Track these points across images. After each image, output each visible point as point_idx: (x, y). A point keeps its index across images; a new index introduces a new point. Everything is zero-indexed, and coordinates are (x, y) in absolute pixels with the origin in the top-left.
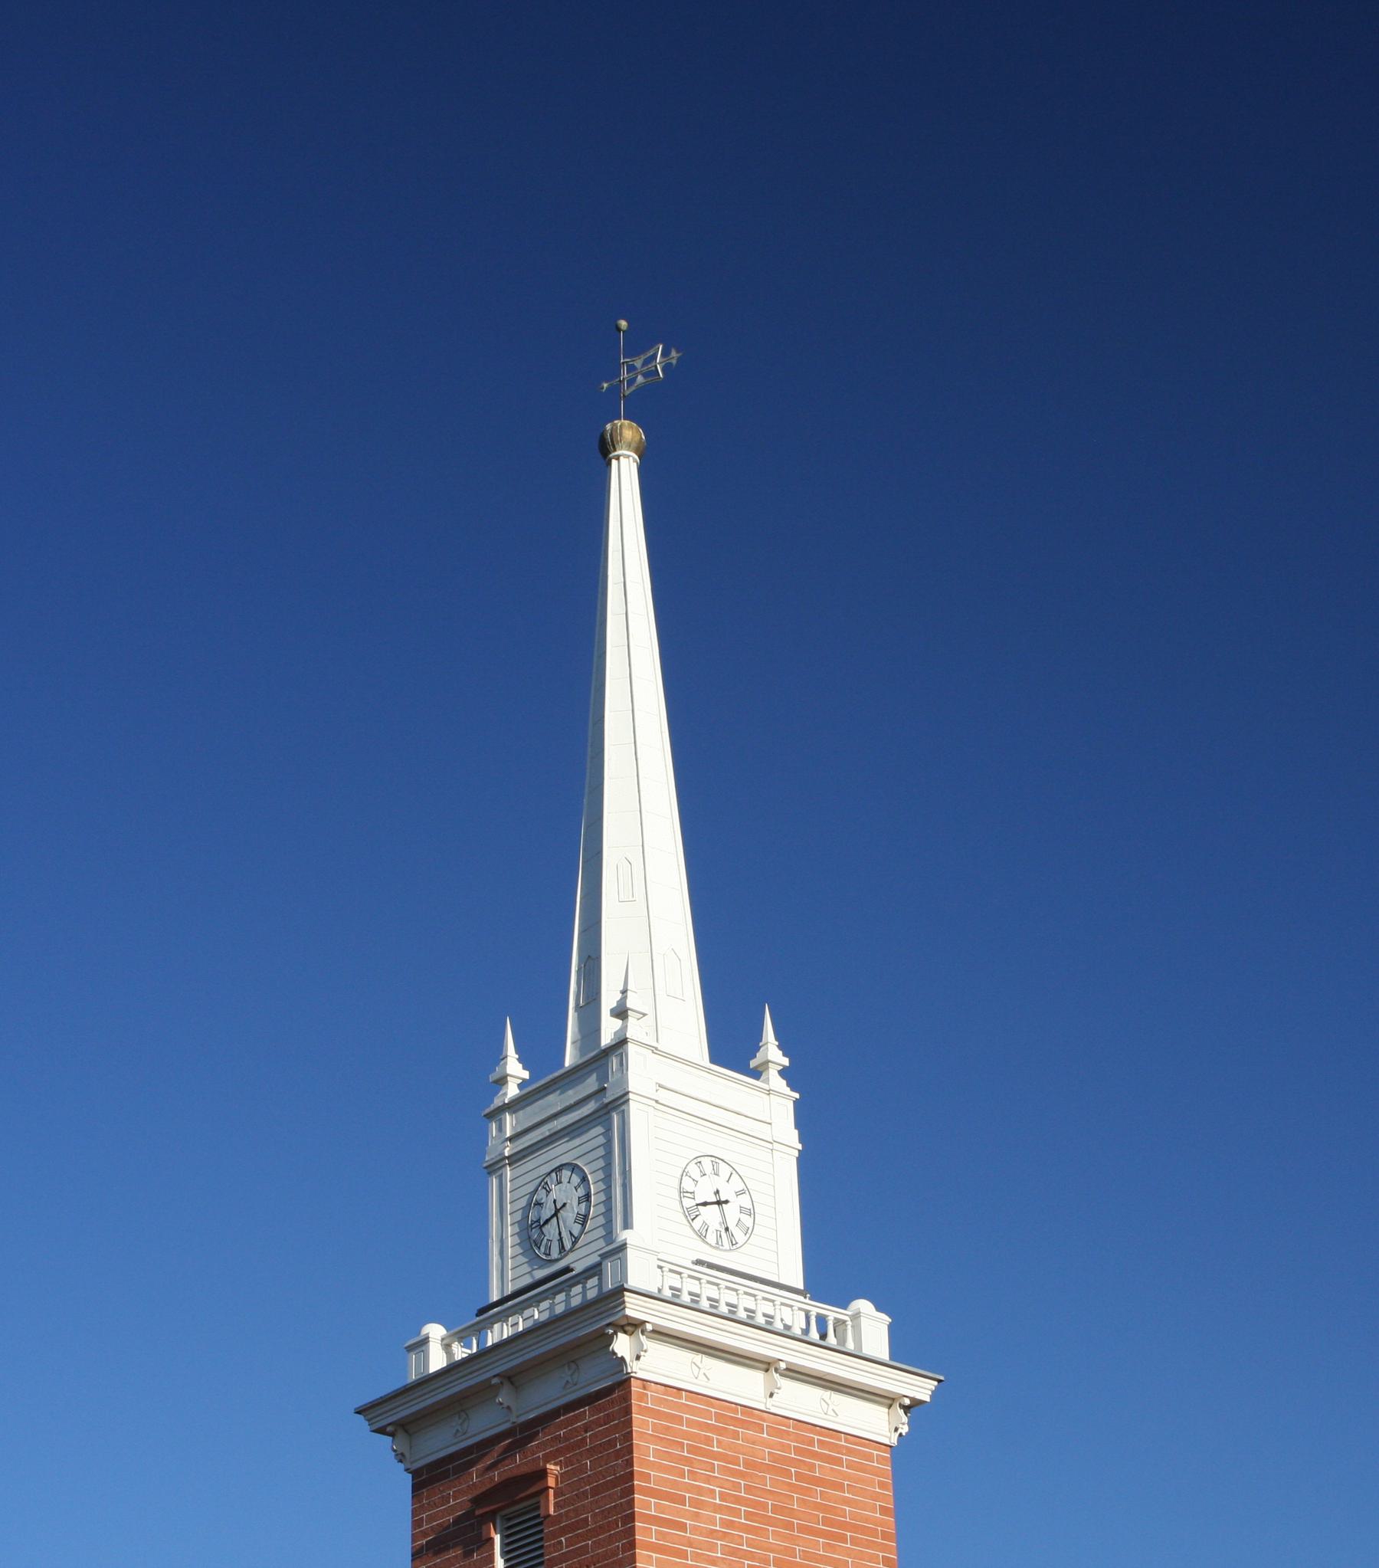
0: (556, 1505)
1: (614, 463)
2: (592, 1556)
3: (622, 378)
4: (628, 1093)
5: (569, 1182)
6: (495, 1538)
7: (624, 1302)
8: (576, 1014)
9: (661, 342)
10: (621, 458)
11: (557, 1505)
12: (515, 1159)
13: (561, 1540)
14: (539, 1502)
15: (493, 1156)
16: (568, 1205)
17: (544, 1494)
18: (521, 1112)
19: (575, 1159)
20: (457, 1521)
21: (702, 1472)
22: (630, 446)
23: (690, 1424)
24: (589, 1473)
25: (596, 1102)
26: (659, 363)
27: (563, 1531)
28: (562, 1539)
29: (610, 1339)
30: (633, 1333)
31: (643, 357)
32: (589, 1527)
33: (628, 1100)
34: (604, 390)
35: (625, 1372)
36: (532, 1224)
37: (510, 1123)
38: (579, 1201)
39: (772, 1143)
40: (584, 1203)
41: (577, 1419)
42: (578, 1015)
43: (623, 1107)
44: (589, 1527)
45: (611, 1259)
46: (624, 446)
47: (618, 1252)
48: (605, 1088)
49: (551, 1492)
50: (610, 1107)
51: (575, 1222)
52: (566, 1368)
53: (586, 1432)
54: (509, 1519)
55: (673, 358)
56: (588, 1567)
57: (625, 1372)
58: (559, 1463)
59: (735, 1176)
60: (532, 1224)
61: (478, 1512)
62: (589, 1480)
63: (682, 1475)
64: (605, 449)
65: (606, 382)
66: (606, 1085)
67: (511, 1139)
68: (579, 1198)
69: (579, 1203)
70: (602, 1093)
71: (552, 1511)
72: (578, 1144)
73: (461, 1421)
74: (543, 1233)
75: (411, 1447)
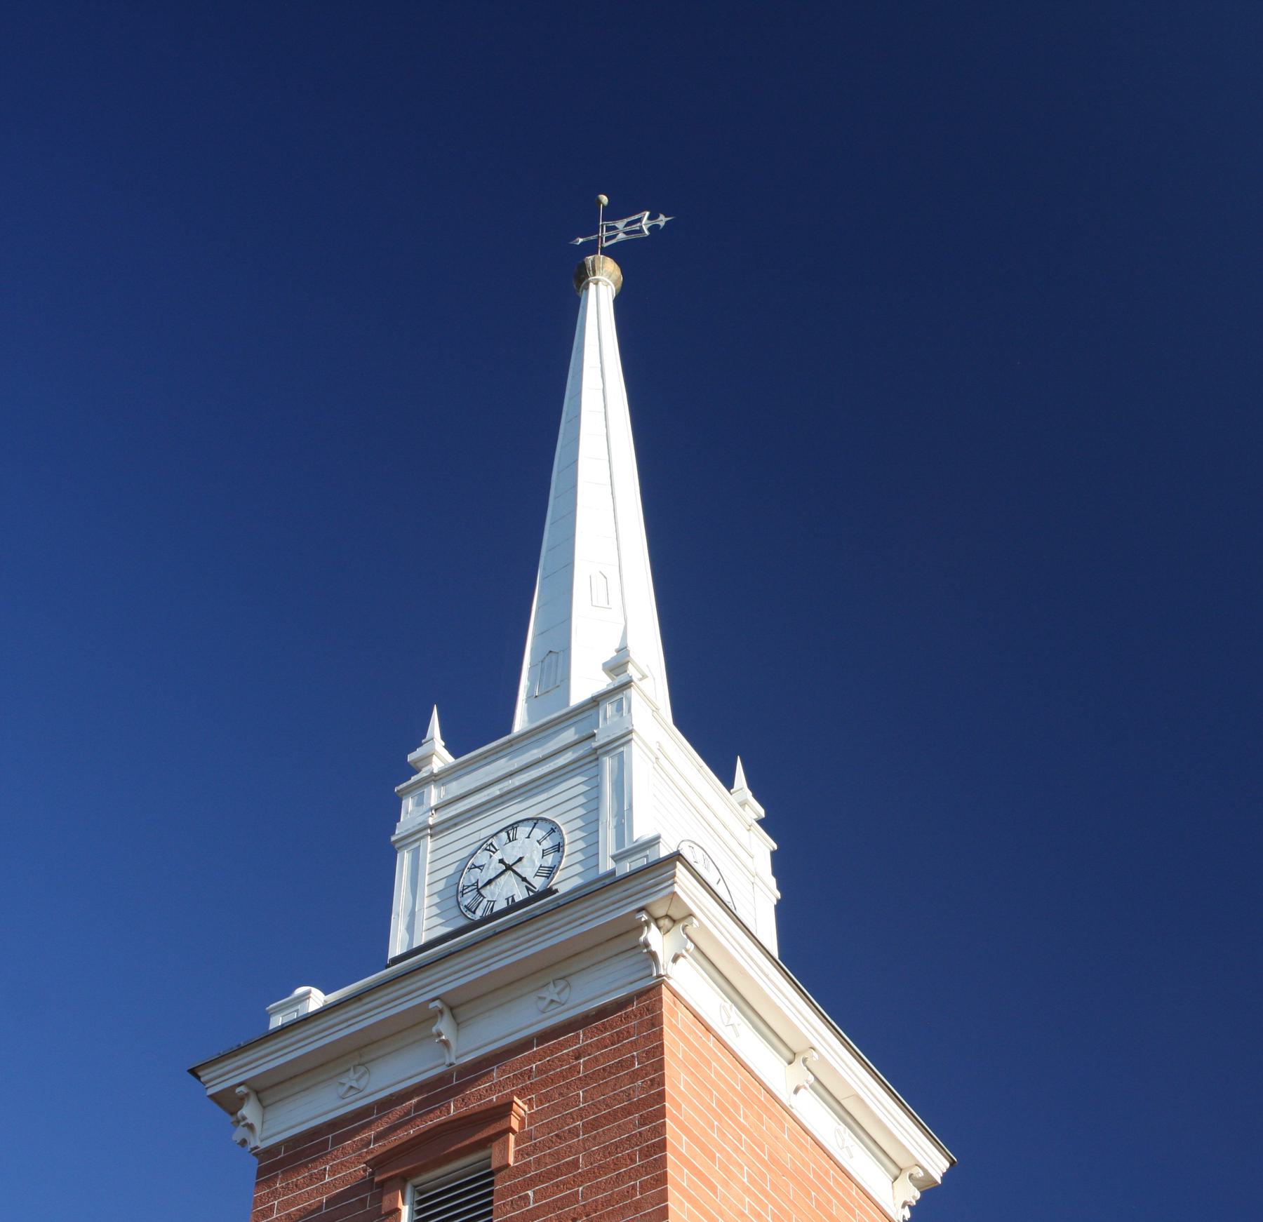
0: (517, 1153)
1: (592, 286)
2: (584, 1205)
3: (600, 235)
4: (631, 732)
5: (528, 837)
6: (403, 1211)
7: (674, 875)
8: (526, 705)
9: (648, 210)
10: (600, 283)
11: (519, 1154)
12: (436, 830)
13: (528, 1194)
14: (490, 1157)
15: (401, 831)
16: (524, 861)
17: (501, 1140)
18: (454, 783)
19: (540, 814)
20: (330, 1201)
21: (730, 1137)
22: (610, 276)
23: (717, 1073)
24: (581, 1106)
25: (573, 753)
26: (645, 224)
27: (530, 1183)
28: (530, 1193)
29: (640, 927)
30: (668, 931)
31: (626, 221)
32: (580, 1170)
33: (630, 740)
34: (578, 244)
35: (655, 975)
36: (463, 890)
37: (434, 795)
38: (543, 853)
39: (754, 877)
40: (552, 855)
41: (562, 1046)
42: (528, 706)
43: (625, 749)
44: (580, 1170)
45: (630, 860)
46: (604, 274)
47: (648, 848)
48: (594, 735)
49: (512, 1137)
50: (599, 752)
51: (536, 875)
52: (551, 986)
53: (577, 1058)
54: (421, 1193)
55: (662, 220)
56: (574, 1220)
57: (655, 975)
58: (529, 1103)
59: (722, 881)
60: (463, 890)
61: (377, 1179)
62: (581, 1114)
63: (712, 1127)
64: (580, 277)
65: (581, 237)
66: (595, 731)
67: (437, 809)
68: (543, 850)
69: (543, 856)
70: (593, 738)
71: (511, 1161)
72: (546, 798)
73: (357, 1076)
74: (482, 895)
75: (263, 1122)
